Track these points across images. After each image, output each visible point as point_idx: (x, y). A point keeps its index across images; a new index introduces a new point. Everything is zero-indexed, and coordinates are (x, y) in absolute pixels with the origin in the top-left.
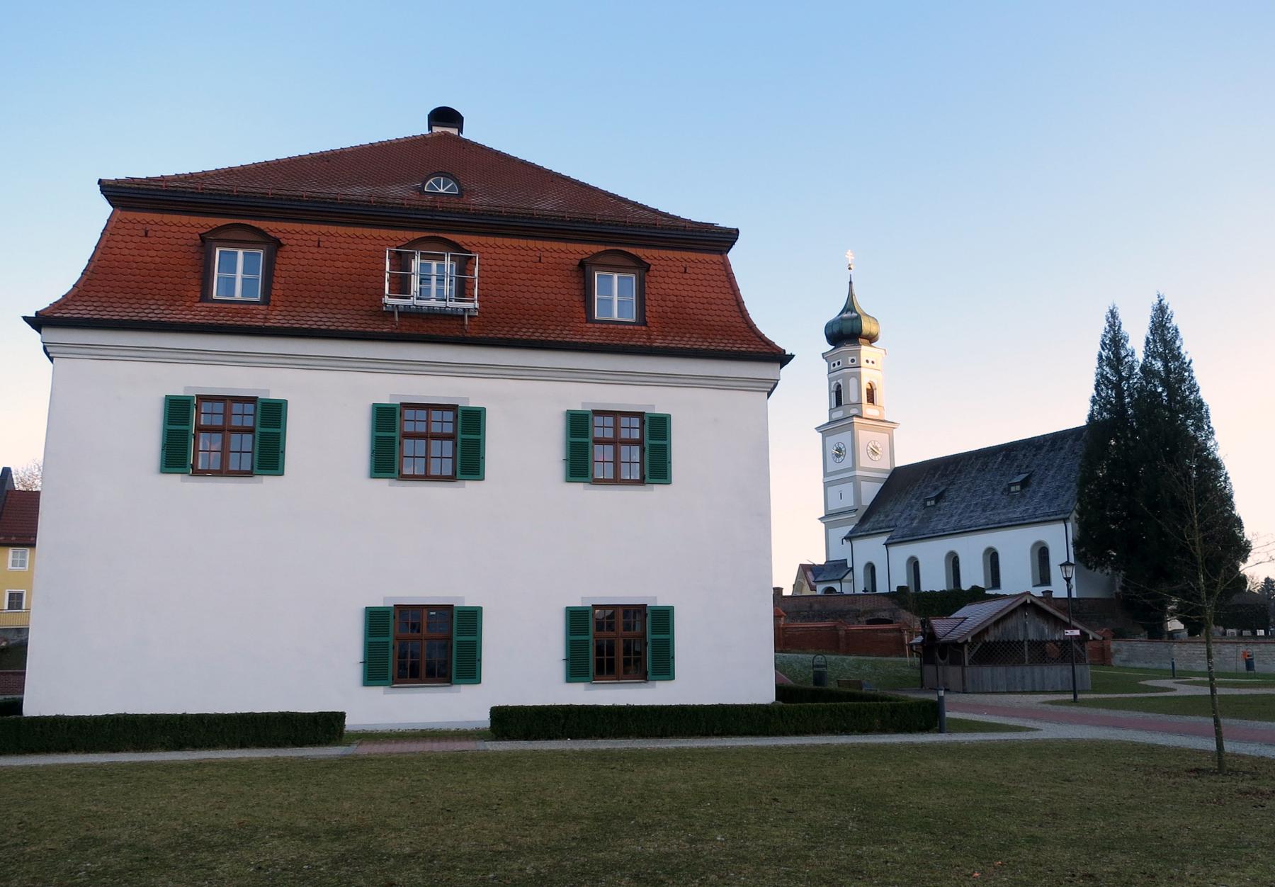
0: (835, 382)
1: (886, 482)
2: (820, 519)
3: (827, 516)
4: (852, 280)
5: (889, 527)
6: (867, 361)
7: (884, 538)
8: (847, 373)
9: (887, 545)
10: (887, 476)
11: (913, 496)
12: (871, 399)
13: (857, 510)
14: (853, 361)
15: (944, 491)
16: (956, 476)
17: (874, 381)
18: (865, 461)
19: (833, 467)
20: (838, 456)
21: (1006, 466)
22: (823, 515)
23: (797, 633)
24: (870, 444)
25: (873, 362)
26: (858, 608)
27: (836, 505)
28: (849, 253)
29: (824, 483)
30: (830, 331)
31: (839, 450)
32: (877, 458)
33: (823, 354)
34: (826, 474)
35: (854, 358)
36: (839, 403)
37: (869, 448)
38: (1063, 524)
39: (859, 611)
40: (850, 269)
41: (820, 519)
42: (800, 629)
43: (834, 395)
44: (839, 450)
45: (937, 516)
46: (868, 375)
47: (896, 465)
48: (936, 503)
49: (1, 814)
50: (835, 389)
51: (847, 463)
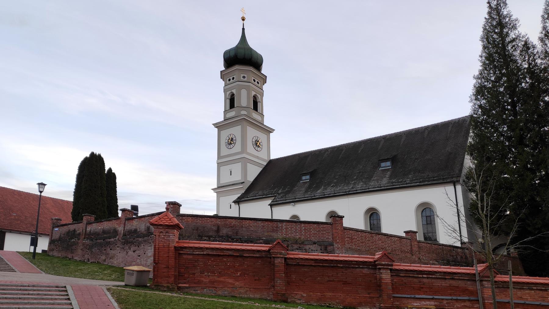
0: (230, 92)
2: (213, 189)
3: (219, 187)
7: (269, 201)
9: (271, 205)
10: (265, 164)
13: (244, 182)
19: (225, 151)
20: (232, 139)
22: (216, 187)
27: (227, 179)
29: (218, 163)
32: (259, 149)
34: (219, 157)
35: (246, 76)
36: (232, 105)
38: (453, 187)
41: (213, 189)
43: (228, 101)
47: (272, 157)
50: (229, 97)
51: (237, 148)
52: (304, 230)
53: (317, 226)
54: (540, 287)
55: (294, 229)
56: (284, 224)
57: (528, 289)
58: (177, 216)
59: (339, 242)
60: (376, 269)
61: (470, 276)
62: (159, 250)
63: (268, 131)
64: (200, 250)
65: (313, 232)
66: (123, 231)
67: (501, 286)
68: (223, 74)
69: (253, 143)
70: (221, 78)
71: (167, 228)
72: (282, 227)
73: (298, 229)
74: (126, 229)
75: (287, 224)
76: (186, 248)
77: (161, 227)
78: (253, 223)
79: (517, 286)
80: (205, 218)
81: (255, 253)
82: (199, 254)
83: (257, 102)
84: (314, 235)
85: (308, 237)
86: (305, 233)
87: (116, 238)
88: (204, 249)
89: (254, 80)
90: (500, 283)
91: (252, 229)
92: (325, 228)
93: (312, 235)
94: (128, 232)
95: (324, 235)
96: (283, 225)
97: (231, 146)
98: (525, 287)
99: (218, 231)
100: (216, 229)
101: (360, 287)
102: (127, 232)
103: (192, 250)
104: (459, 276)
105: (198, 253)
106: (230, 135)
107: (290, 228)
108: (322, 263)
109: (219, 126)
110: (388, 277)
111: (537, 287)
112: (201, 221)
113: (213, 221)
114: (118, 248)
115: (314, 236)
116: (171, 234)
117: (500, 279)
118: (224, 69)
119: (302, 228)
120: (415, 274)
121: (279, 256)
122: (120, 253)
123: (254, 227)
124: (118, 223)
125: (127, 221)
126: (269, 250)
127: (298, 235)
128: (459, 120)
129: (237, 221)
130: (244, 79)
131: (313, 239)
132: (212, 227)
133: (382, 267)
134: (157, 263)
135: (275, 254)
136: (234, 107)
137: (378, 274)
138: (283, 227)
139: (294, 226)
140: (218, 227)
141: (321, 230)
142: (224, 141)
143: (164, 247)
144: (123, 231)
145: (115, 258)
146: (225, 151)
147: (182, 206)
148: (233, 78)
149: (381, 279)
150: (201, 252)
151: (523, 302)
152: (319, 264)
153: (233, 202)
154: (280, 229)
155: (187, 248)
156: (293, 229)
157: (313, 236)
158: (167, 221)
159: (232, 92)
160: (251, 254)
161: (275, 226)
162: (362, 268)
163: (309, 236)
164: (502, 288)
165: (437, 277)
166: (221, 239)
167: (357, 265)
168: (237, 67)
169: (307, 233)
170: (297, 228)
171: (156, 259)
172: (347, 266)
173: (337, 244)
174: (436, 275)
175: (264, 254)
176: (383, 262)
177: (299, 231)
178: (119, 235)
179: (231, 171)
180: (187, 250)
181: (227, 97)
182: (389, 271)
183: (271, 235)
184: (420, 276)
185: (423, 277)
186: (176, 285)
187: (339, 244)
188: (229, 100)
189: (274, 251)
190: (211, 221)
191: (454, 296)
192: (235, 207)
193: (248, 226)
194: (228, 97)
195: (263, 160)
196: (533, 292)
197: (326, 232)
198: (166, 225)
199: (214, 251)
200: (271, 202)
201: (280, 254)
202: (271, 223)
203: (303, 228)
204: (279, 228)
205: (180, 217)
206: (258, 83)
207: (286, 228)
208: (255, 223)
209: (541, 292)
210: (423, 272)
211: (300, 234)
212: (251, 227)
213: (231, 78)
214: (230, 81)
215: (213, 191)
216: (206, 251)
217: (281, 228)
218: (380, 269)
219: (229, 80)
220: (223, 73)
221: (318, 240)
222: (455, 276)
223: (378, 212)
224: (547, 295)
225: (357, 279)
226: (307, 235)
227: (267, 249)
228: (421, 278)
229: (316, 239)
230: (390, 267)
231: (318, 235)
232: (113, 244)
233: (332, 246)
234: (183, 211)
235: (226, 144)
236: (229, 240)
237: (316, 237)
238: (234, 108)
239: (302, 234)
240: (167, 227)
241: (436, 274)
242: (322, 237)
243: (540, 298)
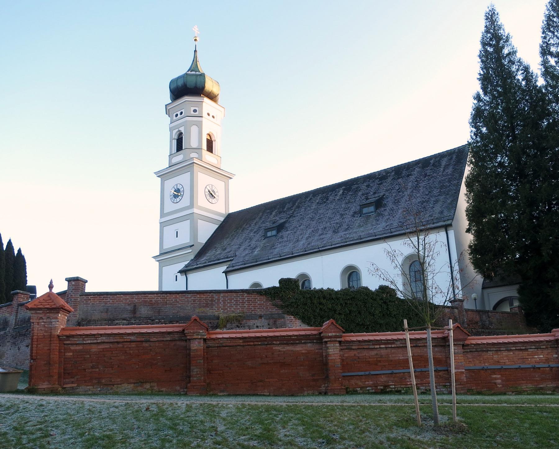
0: (177, 130)
1: (221, 224)
2: (154, 257)
3: (161, 254)
4: (197, 50)
5: (227, 258)
6: (208, 114)
7: (224, 268)
8: (189, 121)
9: (226, 273)
10: (222, 219)
11: (251, 231)
12: (210, 148)
14: (195, 111)
15: (285, 222)
16: (295, 211)
17: (213, 132)
18: (202, 200)
19: (170, 206)
20: (176, 196)
21: (349, 196)
23: (95, 349)
24: (208, 187)
25: (213, 117)
26: (216, 314)
27: (171, 243)
28: (196, 27)
30: (174, 86)
31: (178, 191)
32: (214, 201)
33: (166, 105)
36: (179, 147)
37: (207, 191)
39: (218, 318)
40: (195, 40)
41: (154, 257)
42: (104, 339)
43: (175, 143)
44: (178, 191)
45: (280, 243)
46: (208, 126)
48: (278, 232)
49: (1, 425)
50: (176, 137)
51: (185, 201)
52: (247, 301)
54: (519, 346)
55: (235, 301)
56: (222, 295)
57: (506, 350)
58: (80, 295)
60: (322, 343)
61: (437, 341)
62: (37, 341)
63: (227, 177)
64: (93, 338)
65: (258, 303)
66: (15, 320)
67: (474, 350)
68: (169, 108)
69: (206, 194)
70: (167, 114)
71: (47, 313)
72: (219, 299)
74: (18, 318)
75: (225, 295)
76: (73, 336)
77: (41, 312)
78: (181, 298)
79: (493, 348)
80: (118, 296)
81: (165, 336)
82: (91, 343)
83: (212, 141)
84: (259, 306)
85: (253, 309)
86: (248, 305)
87: (6, 331)
88: (97, 336)
90: (473, 346)
91: (180, 305)
93: (257, 306)
94: (21, 321)
96: (220, 297)
97: (178, 199)
98: (502, 349)
99: (134, 311)
100: (132, 309)
101: (302, 367)
102: (20, 321)
103: (81, 339)
104: (423, 342)
105: (89, 342)
106: (177, 185)
108: (253, 342)
109: (163, 175)
110: (336, 352)
111: (516, 347)
112: (111, 299)
113: (128, 299)
114: (8, 344)
116: (54, 320)
117: (474, 342)
118: (171, 102)
120: (370, 345)
121: (195, 337)
122: (10, 349)
123: (183, 302)
124: (9, 311)
125: (20, 307)
126: (184, 330)
127: (239, 309)
128: (447, 153)
129: (159, 296)
130: (195, 113)
131: (258, 312)
132: (127, 307)
133: (329, 340)
134: (35, 359)
135: (190, 336)
136: (182, 149)
137: (325, 349)
138: (220, 299)
139: (234, 297)
140: (135, 306)
143: (44, 338)
144: (14, 321)
145: (4, 357)
146: (170, 206)
147: (88, 282)
148: (181, 113)
149: (327, 356)
150: (94, 340)
151: (499, 367)
152: (249, 344)
153: (178, 272)
154: (216, 303)
155: (75, 337)
156: (233, 301)
157: (259, 308)
158: (48, 303)
159: (179, 131)
160: (160, 337)
161: (210, 299)
162: (304, 343)
163: (254, 308)
164: (476, 353)
165: (398, 346)
166: (138, 321)
167: (297, 340)
168: (186, 99)
169: (252, 304)
170: (238, 299)
171: (33, 354)
172: (285, 342)
174: (396, 344)
175: (176, 336)
176: (330, 333)
178: (10, 327)
179: (177, 232)
180: (76, 339)
181: (173, 137)
182: (338, 345)
183: (204, 311)
184: (376, 347)
185: (380, 348)
186: (61, 385)
188: (176, 140)
189: (189, 331)
190: (126, 299)
191: (418, 368)
192: (182, 278)
193: (174, 302)
194: (174, 136)
195: (220, 214)
196: (512, 353)
198: (47, 308)
199: (111, 338)
200: (226, 268)
201: (197, 335)
202: (205, 295)
203: (246, 299)
204: (215, 301)
205: (84, 297)
207: (248, 301)
208: (183, 298)
209: (521, 353)
210: (380, 342)
211: (242, 307)
212: (179, 302)
213: (179, 113)
214: (177, 117)
215: (155, 260)
216: (100, 339)
217: (218, 301)
218: (326, 342)
219: (177, 115)
220: (168, 107)
221: (265, 313)
222: (419, 343)
223: (359, 271)
224: (528, 356)
225: (298, 358)
226: (251, 307)
227: (181, 329)
228: (378, 349)
229: (262, 312)
230: (338, 339)
231: (265, 306)
232: (2, 339)
233: (282, 319)
234: (89, 288)
235: (171, 197)
236: (148, 322)
237: (263, 309)
238: (182, 151)
239: (245, 307)
240: (48, 311)
241: (397, 343)
242: (270, 308)
243: (520, 360)
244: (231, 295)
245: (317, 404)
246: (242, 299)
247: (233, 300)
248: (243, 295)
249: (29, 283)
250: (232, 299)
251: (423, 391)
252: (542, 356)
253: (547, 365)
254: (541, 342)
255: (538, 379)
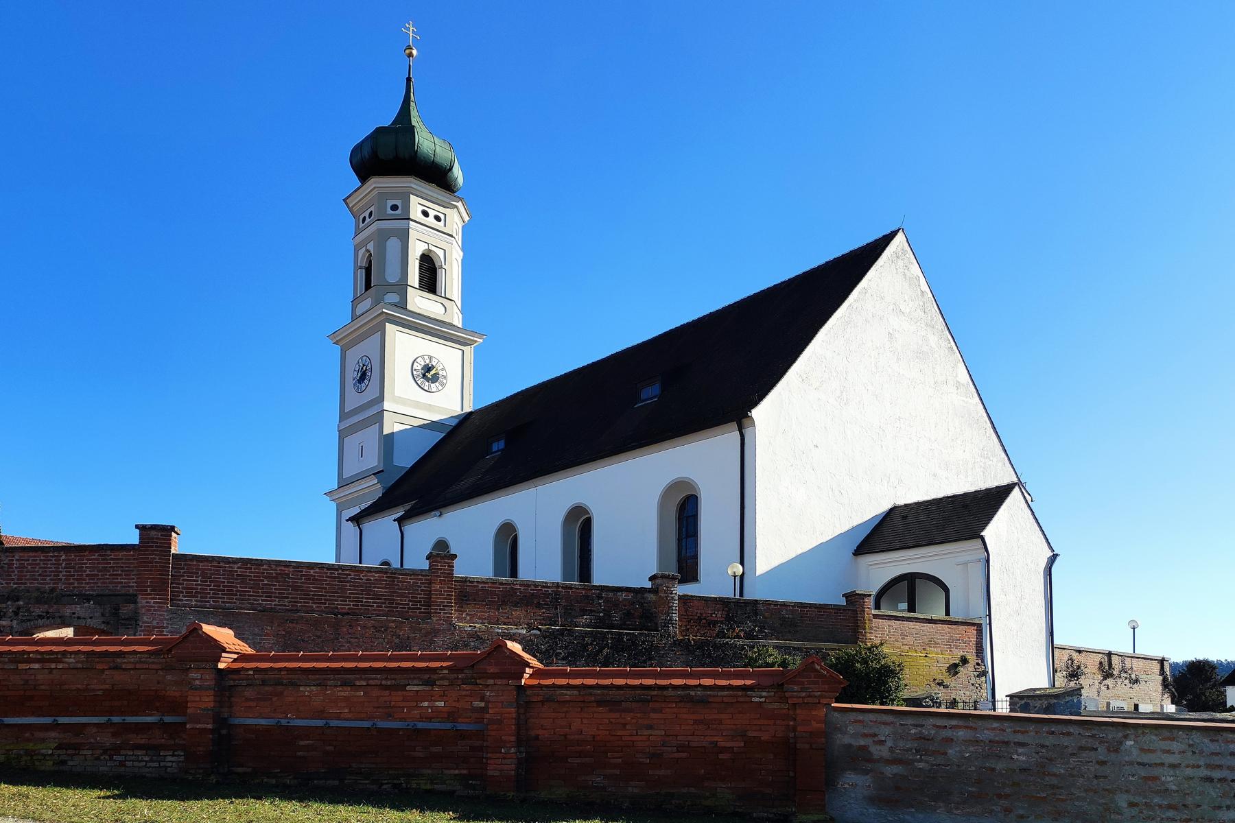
2: (328, 494)
9: (400, 521)
34: (343, 415)
38: (736, 435)
41: (328, 494)
53: (98, 555)
55: (40, 568)
59: (150, 594)
65: (88, 572)
69: (415, 373)
72: (10, 565)
73: (51, 568)
84: (89, 579)
89: (425, 214)
92: (122, 559)
95: (117, 579)
96: (13, 560)
106: (362, 358)
107: (29, 567)
115: (91, 583)
119: (61, 564)
130: (393, 212)
139: (41, 560)
141: (111, 567)
142: (352, 375)
173: (146, 598)
177: (54, 572)
187: (150, 599)
188: (364, 270)
197: (122, 571)
206: (437, 218)
209: (387, 693)
217: (8, 568)
224: (403, 701)
229: (95, 590)
234: (179, 546)
243: (380, 710)
244: (35, 556)
245: (578, 760)
246: (55, 564)
247: (38, 567)
248: (57, 556)
249: (133, 538)
250: (35, 564)
251: (1020, 750)
252: (442, 704)
253: (448, 726)
254: (435, 670)
255: (421, 755)
